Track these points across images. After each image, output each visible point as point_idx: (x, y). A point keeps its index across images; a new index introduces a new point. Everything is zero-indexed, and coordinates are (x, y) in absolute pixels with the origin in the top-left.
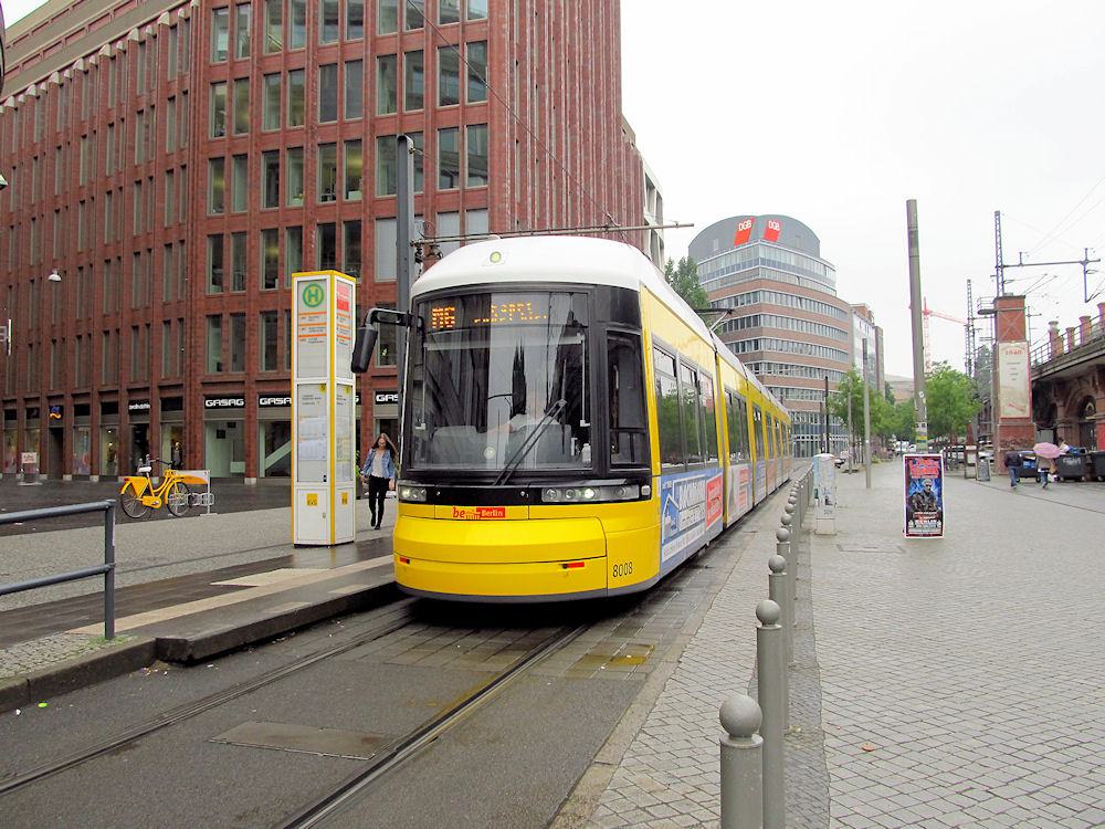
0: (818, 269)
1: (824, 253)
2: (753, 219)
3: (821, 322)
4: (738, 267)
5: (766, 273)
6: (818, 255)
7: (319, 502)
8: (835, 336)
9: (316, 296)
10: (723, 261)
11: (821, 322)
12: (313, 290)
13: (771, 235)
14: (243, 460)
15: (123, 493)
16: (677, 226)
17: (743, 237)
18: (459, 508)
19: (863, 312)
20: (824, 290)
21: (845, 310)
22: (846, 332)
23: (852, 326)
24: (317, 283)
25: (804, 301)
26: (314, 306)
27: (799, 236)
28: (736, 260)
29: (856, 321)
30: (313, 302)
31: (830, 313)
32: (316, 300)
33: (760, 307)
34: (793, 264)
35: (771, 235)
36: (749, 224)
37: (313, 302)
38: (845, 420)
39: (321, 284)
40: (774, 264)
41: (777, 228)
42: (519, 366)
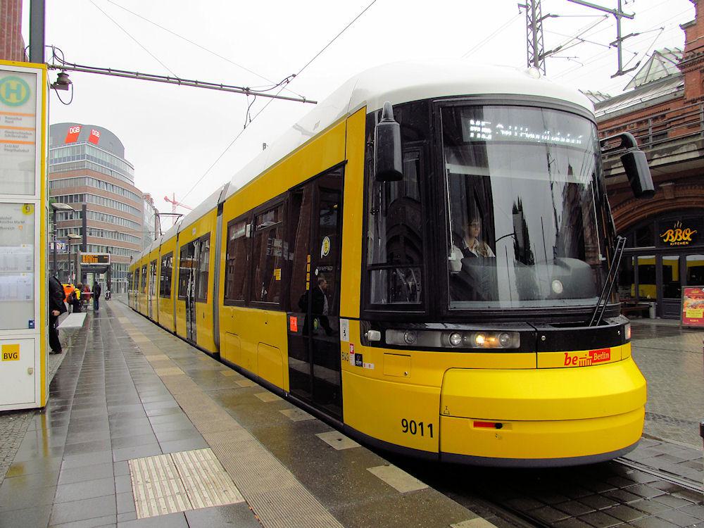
0: (122, 166)
1: (127, 157)
2: (81, 126)
3: (125, 203)
4: (69, 159)
5: (89, 165)
6: (123, 157)
7: (22, 354)
8: (129, 211)
9: (18, 92)
10: (65, 152)
11: (125, 203)
12: (14, 84)
13: (93, 140)
14: (679, 295)
15: (308, 289)
16: (304, 101)
17: (72, 138)
18: (572, 354)
19: (148, 198)
20: (127, 181)
21: (136, 193)
22: (140, 211)
23: (143, 208)
24: (21, 77)
25: (101, 183)
26: (16, 105)
27: (112, 144)
28: (67, 153)
29: (146, 204)
30: (13, 98)
31: (128, 196)
32: (19, 97)
33: (86, 188)
34: (108, 161)
35: (93, 140)
36: (77, 130)
37: (13, 98)
38: (560, 297)
39: (29, 81)
40: (96, 160)
41: (98, 135)
42: (518, 210)
